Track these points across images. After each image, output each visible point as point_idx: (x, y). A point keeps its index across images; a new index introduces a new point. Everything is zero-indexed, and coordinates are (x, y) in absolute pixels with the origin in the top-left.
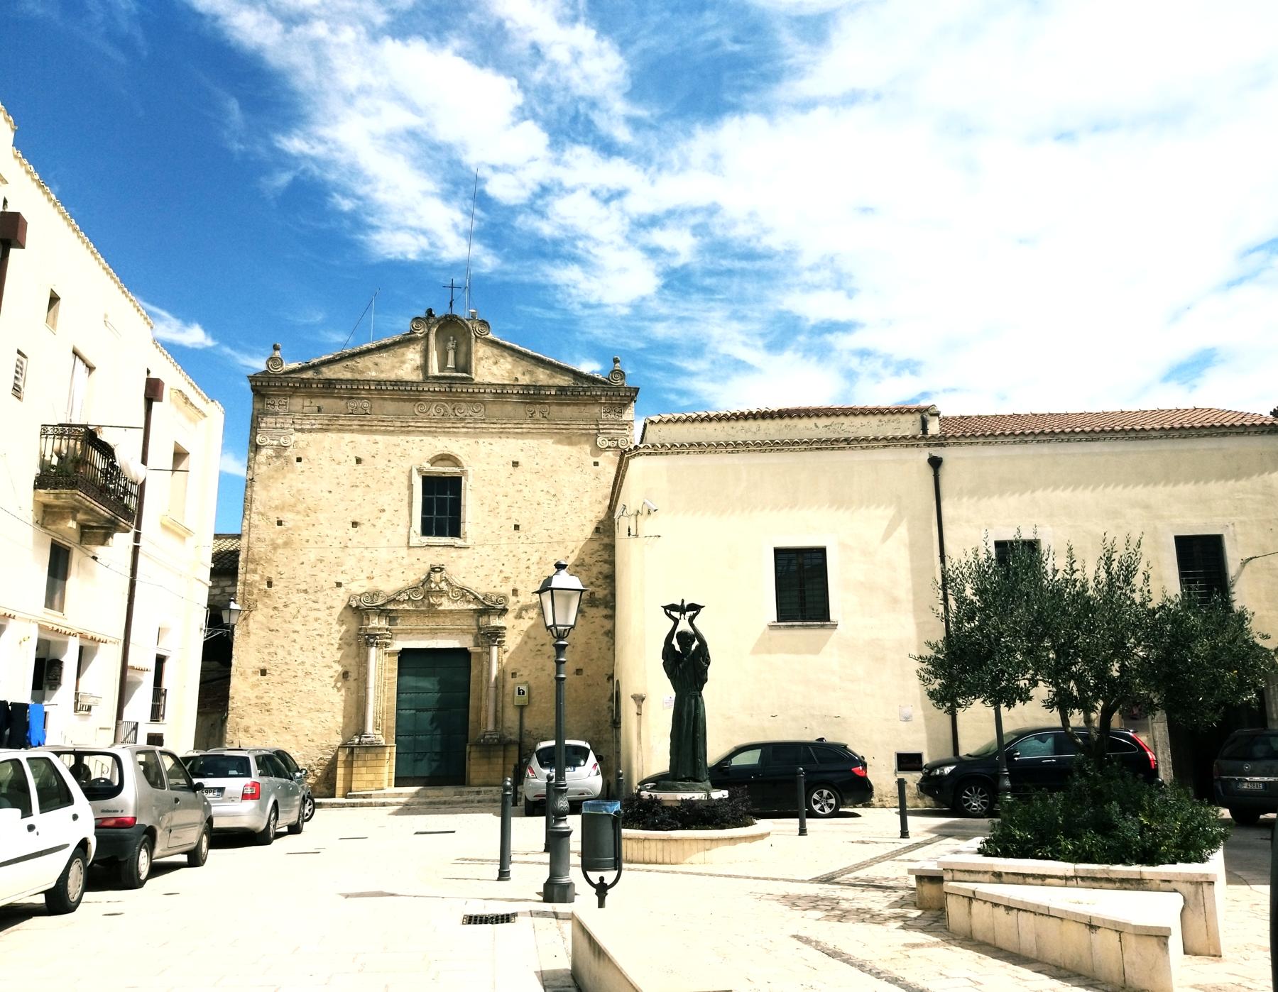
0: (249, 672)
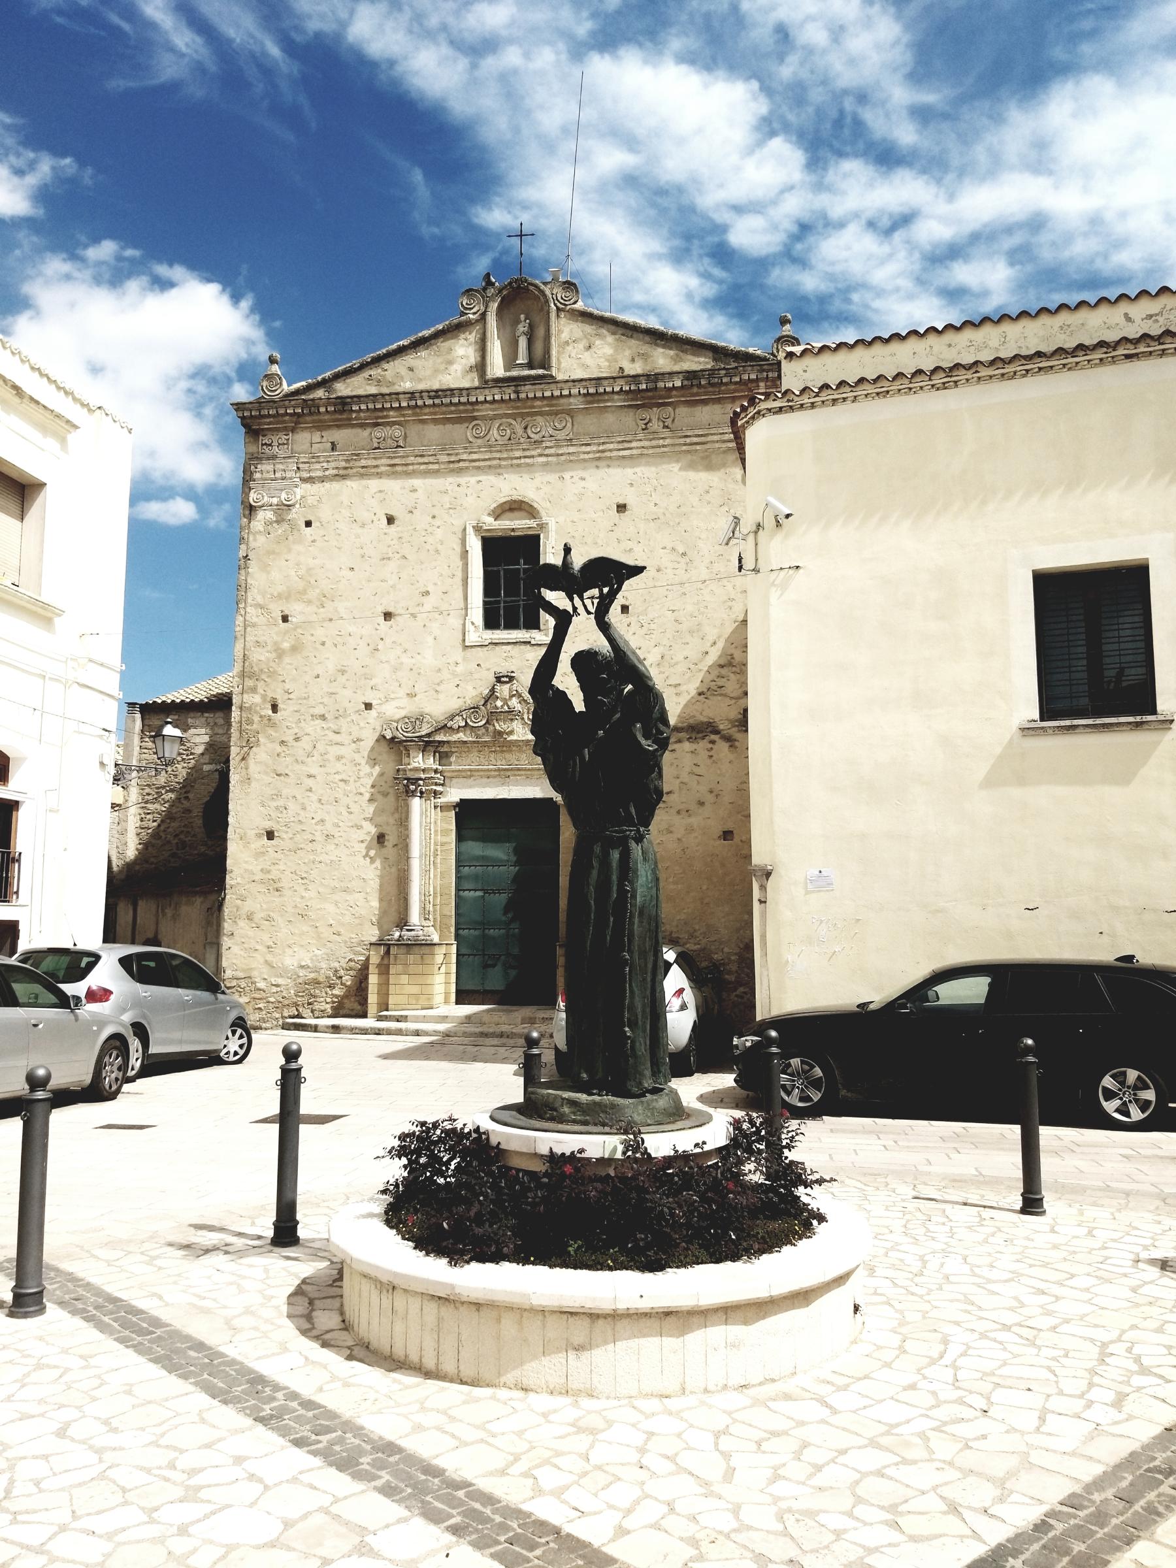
0: (251, 834)
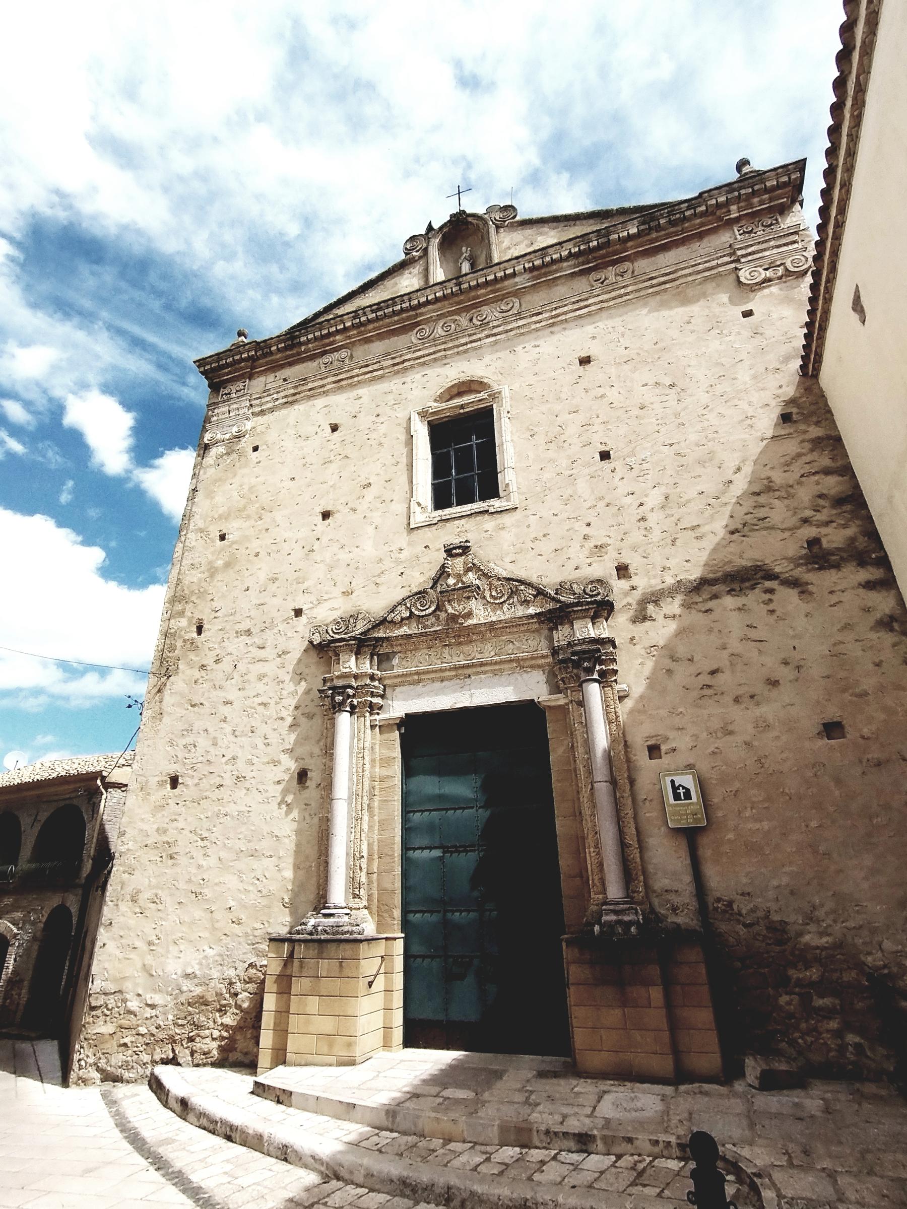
0: (153, 781)
